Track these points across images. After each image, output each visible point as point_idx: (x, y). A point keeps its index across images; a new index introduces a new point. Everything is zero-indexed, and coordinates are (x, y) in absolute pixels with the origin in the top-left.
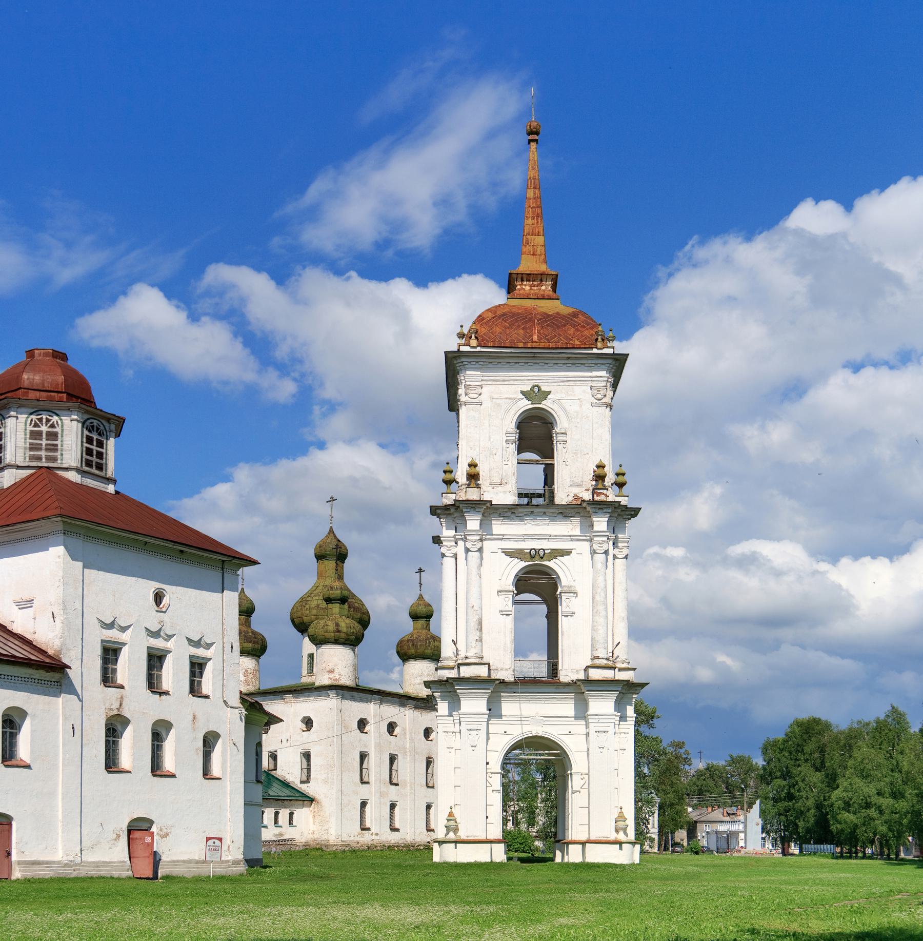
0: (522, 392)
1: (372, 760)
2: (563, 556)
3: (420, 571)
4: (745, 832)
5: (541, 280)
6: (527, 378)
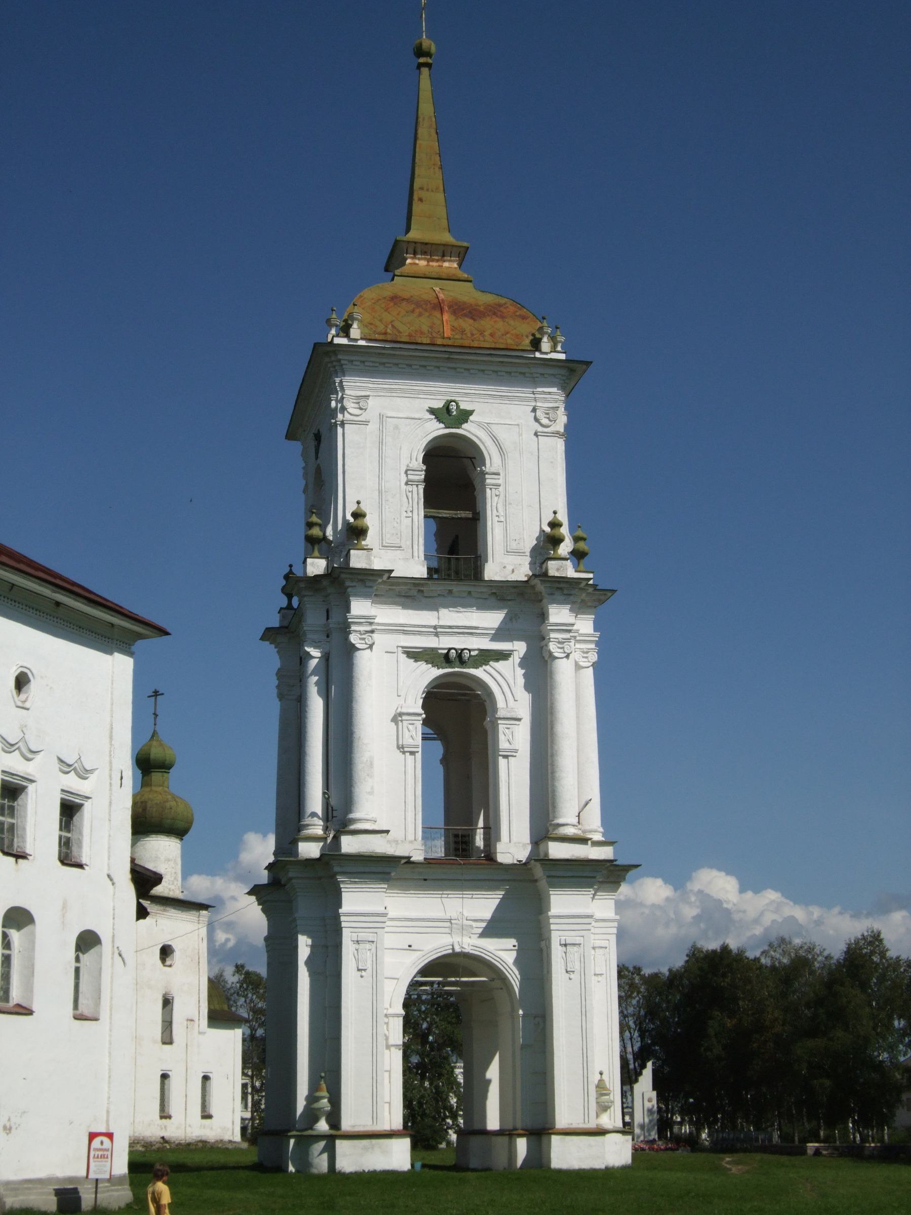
0: (432, 411)
1: (175, 1084)
2: (497, 660)
3: (156, 694)
4: (470, 650)
5: (443, 256)
6: (438, 392)
